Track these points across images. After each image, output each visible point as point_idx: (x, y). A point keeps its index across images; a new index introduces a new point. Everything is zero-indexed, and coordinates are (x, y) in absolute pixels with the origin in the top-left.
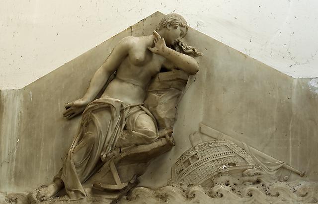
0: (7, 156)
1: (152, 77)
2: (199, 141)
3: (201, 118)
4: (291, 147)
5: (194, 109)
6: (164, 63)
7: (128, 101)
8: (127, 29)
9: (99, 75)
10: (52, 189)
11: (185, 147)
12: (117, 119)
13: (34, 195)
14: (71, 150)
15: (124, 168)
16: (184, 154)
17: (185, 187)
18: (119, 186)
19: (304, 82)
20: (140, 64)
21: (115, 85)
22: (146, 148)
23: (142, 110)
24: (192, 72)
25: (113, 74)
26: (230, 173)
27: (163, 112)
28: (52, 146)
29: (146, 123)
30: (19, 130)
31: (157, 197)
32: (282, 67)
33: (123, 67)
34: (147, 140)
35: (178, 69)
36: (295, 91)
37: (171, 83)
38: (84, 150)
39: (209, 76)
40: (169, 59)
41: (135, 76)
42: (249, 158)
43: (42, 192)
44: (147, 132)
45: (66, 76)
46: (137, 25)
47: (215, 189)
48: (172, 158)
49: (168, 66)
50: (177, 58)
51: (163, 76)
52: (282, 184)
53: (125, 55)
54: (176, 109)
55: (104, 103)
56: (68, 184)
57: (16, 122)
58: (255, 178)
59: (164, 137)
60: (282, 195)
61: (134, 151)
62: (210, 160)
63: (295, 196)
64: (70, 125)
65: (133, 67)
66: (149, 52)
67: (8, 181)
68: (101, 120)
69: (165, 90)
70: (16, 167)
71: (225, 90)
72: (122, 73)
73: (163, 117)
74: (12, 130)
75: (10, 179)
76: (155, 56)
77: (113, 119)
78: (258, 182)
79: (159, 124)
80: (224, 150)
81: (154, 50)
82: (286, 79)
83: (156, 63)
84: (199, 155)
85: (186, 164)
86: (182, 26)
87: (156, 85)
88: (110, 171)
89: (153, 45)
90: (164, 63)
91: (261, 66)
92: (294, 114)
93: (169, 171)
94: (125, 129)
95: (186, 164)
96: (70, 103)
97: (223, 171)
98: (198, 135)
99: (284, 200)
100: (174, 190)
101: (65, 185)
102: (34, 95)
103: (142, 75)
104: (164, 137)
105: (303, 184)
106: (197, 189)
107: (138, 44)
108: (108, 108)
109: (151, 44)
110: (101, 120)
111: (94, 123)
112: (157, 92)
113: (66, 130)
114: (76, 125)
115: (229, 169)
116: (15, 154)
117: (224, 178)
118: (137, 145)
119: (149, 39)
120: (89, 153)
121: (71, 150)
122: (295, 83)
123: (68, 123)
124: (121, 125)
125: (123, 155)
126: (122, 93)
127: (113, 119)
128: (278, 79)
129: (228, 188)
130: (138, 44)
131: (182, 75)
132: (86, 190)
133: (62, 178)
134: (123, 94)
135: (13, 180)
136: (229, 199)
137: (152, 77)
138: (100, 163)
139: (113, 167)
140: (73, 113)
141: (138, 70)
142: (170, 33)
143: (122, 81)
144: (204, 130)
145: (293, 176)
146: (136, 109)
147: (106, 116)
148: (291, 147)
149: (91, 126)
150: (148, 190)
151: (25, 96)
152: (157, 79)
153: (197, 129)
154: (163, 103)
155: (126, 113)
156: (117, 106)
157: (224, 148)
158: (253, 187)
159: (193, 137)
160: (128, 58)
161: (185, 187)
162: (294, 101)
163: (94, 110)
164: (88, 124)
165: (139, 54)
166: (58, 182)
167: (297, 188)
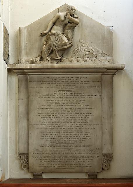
0: (23, 47)
1: (66, 25)
2: (79, 44)
3: (80, 37)
4: (105, 47)
5: (78, 33)
6: (69, 21)
7: (59, 32)
8: (132, 76)
9: (51, 23)
10: (39, 58)
11: (75, 46)
12: (57, 38)
13: (34, 60)
14: (44, 47)
15: (59, 52)
16: (75, 48)
17: (76, 58)
18: (59, 58)
19: (108, 27)
20: (63, 21)
21: (55, 27)
22: (66, 47)
23: (63, 35)
24: (78, 24)
25: (54, 24)
26: (89, 54)
27: (70, 36)
28: (37, 45)
29: (65, 39)
30: (27, 39)
31: (69, 61)
32: (101, 22)
33: (57, 21)
34: (66, 45)
35: (74, 23)
36: (106, 30)
37: (71, 27)
38: (48, 47)
39: (82, 25)
40: (71, 20)
41: (61, 24)
42: (94, 50)
43: (36, 60)
44: (66, 42)
45: (39, 23)
46: (60, 8)
47: (85, 59)
48: (72, 49)
49: (70, 22)
50: (74, 20)
51: (69, 25)
52: (103, 58)
53: (58, 18)
54: (73, 35)
55: (53, 33)
56: (44, 57)
57: (25, 37)
58: (96, 56)
59: (70, 43)
60: (103, 61)
61: (62, 48)
62: (83, 50)
63: (107, 61)
64: (42, 38)
65: (61, 22)
66: (65, 17)
67: (24, 55)
68: (52, 38)
69: (70, 29)
70: (27, 51)
71: (86, 29)
72: (57, 23)
73: (70, 37)
74: (24, 39)
75: (25, 55)
76: (67, 18)
77: (56, 38)
78: (96, 57)
79: (68, 39)
80: (87, 48)
81: (67, 17)
82: (103, 26)
83: (67, 21)
84: (80, 49)
85: (76, 51)
86: (74, 10)
87: (67, 27)
88: (56, 53)
89: (66, 16)
90: (69, 21)
91: (97, 22)
92: (106, 37)
93: (71, 53)
94: (59, 41)
95: (76, 51)
96: (42, 32)
97: (87, 54)
98: (79, 42)
99: (104, 63)
100: (73, 59)
101: (43, 57)
102: (31, 28)
103: (63, 24)
104: (70, 43)
105: (109, 58)
106: (80, 59)
107: (62, 15)
108: (54, 34)
109: (66, 15)
110: (52, 38)
111: (50, 39)
112: (68, 29)
113: (41, 40)
114: (44, 38)
115: (88, 53)
116: (26, 47)
117: (87, 56)
118: (63, 46)
119: (65, 13)
120: (49, 48)
121: (44, 47)
122: (106, 28)
123: (41, 38)
124: (58, 39)
125: (59, 49)
126: (57, 30)
127: (56, 38)
128: (101, 26)
129: (88, 59)
130: (62, 15)
131: (75, 25)
132: (49, 59)
133: (42, 55)
134: (57, 30)
135: (26, 55)
136: (89, 62)
137: (66, 25)
138: (52, 51)
139: (56, 52)
140: (42, 35)
141: (62, 22)
142: (71, 11)
143: (57, 26)
144: (81, 41)
145: (106, 55)
146: (62, 35)
147: (54, 37)
148: (105, 47)
149: (49, 39)
150: (66, 59)
151: (28, 29)
152: (67, 26)
153: (79, 41)
154: (69, 33)
155: (59, 36)
156: (57, 34)
157: (87, 47)
158: (95, 59)
159: (78, 43)
160: (59, 19)
161: (76, 58)
162: (106, 33)
163: (50, 35)
164: (48, 39)
165: (62, 18)
166: (40, 56)
167: (107, 59)
